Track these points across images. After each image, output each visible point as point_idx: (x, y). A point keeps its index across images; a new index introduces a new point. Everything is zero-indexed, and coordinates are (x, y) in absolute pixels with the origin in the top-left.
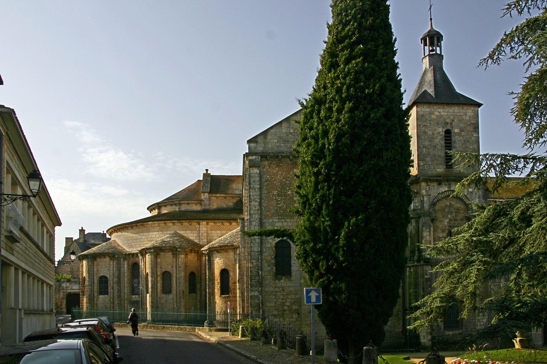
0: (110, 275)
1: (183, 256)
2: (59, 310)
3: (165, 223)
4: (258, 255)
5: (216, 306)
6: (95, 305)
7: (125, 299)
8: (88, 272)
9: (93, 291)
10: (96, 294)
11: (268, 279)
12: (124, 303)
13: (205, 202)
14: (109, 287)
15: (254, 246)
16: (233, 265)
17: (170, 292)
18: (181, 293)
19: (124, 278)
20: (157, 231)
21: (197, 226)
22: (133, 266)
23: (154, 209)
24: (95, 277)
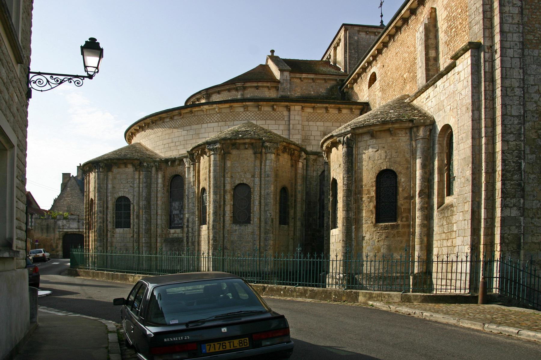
0: (134, 196)
1: (273, 156)
2: (54, 253)
4: (519, 124)
5: (364, 245)
6: (109, 245)
7: (157, 236)
8: (98, 189)
9: (105, 221)
10: (110, 227)
11: (531, 181)
12: (156, 242)
13: (285, 85)
14: (132, 216)
15: (511, 103)
16: (408, 162)
17: (248, 221)
18: (269, 222)
19: (157, 201)
20: (216, 122)
21: (286, 113)
22: (172, 181)
24: (109, 198)
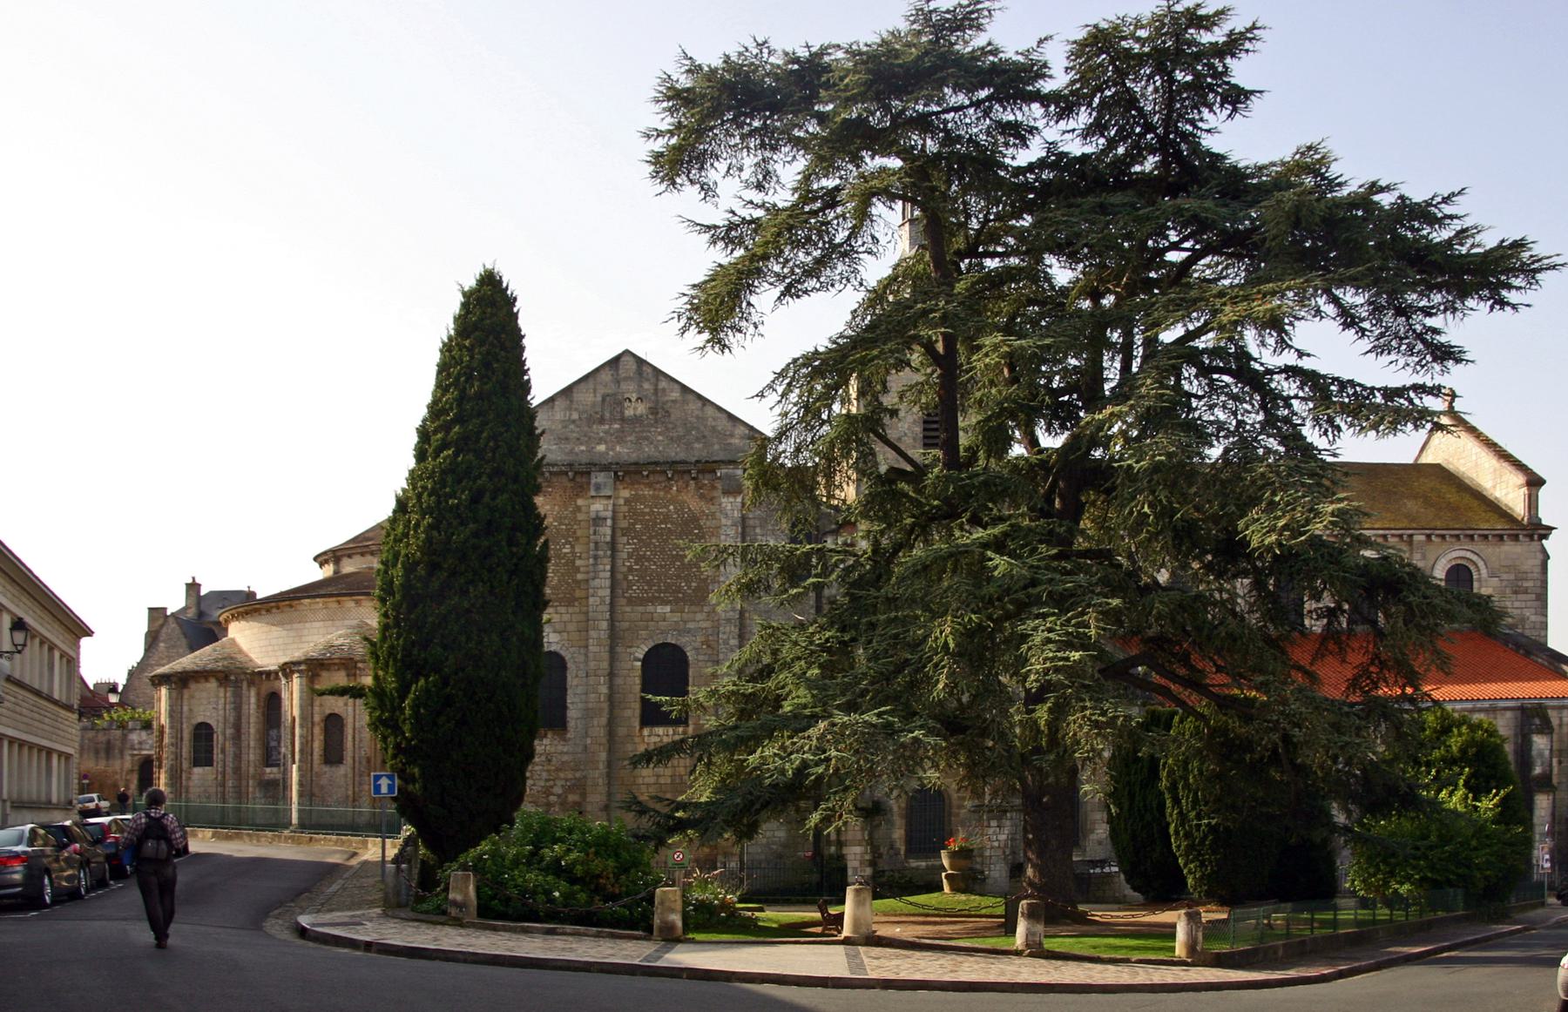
3: (339, 602)
10: (185, 765)
18: (364, 763)
23: (326, 562)
24: (185, 726)
